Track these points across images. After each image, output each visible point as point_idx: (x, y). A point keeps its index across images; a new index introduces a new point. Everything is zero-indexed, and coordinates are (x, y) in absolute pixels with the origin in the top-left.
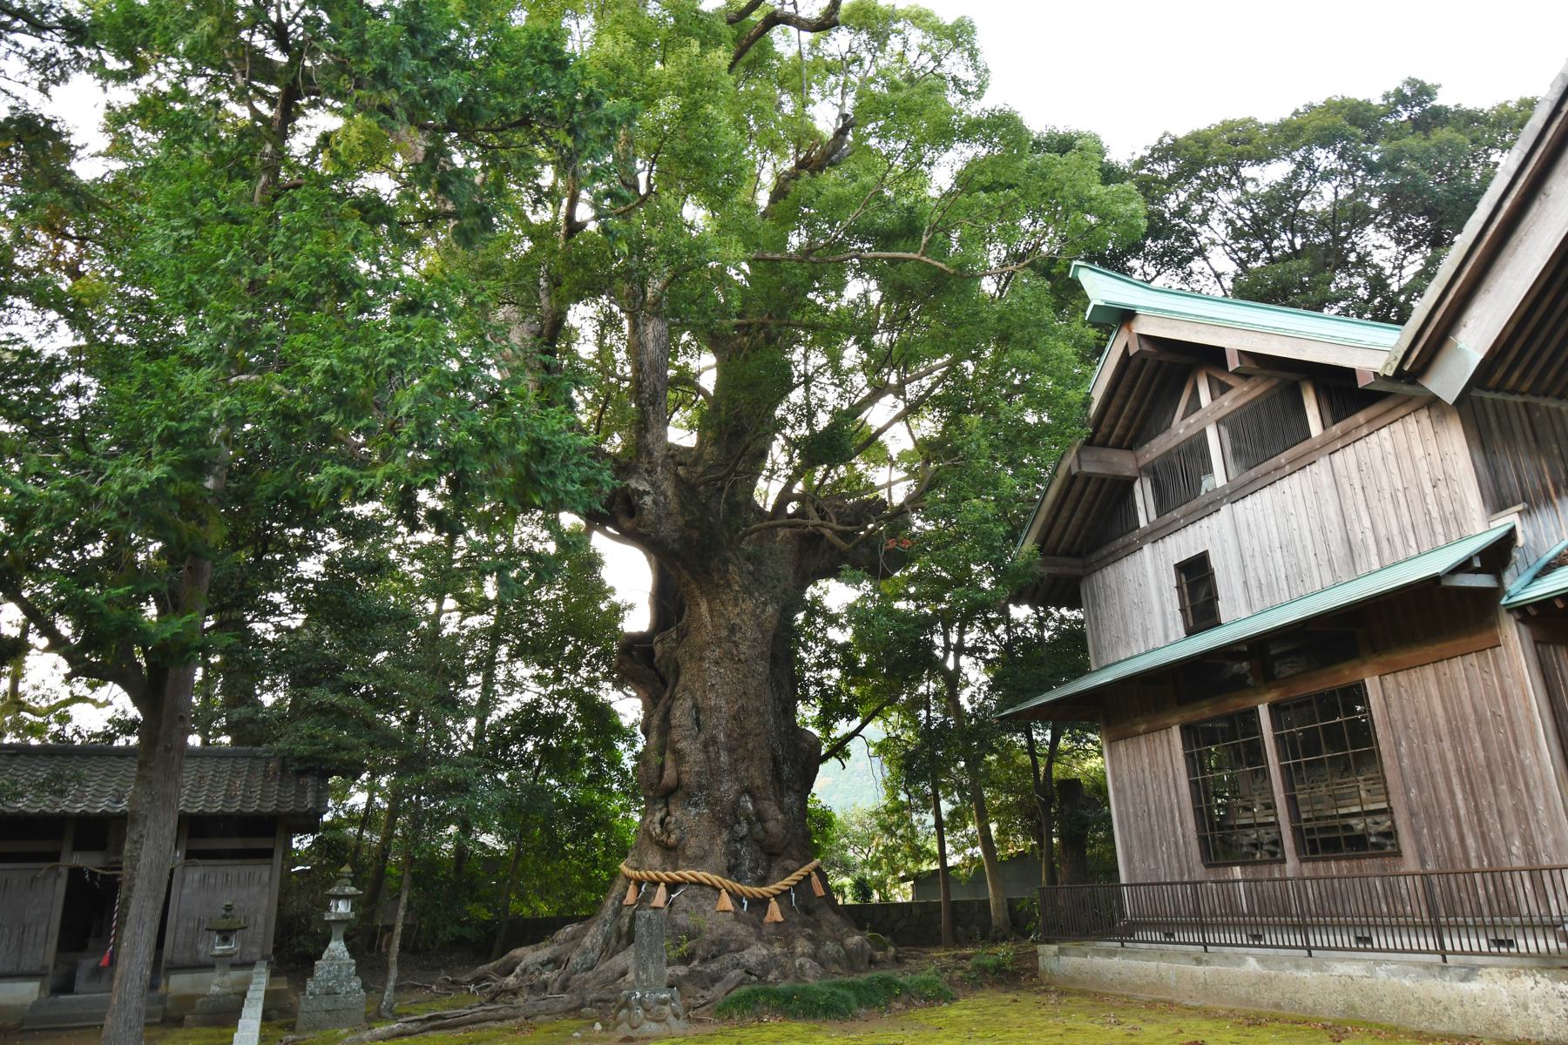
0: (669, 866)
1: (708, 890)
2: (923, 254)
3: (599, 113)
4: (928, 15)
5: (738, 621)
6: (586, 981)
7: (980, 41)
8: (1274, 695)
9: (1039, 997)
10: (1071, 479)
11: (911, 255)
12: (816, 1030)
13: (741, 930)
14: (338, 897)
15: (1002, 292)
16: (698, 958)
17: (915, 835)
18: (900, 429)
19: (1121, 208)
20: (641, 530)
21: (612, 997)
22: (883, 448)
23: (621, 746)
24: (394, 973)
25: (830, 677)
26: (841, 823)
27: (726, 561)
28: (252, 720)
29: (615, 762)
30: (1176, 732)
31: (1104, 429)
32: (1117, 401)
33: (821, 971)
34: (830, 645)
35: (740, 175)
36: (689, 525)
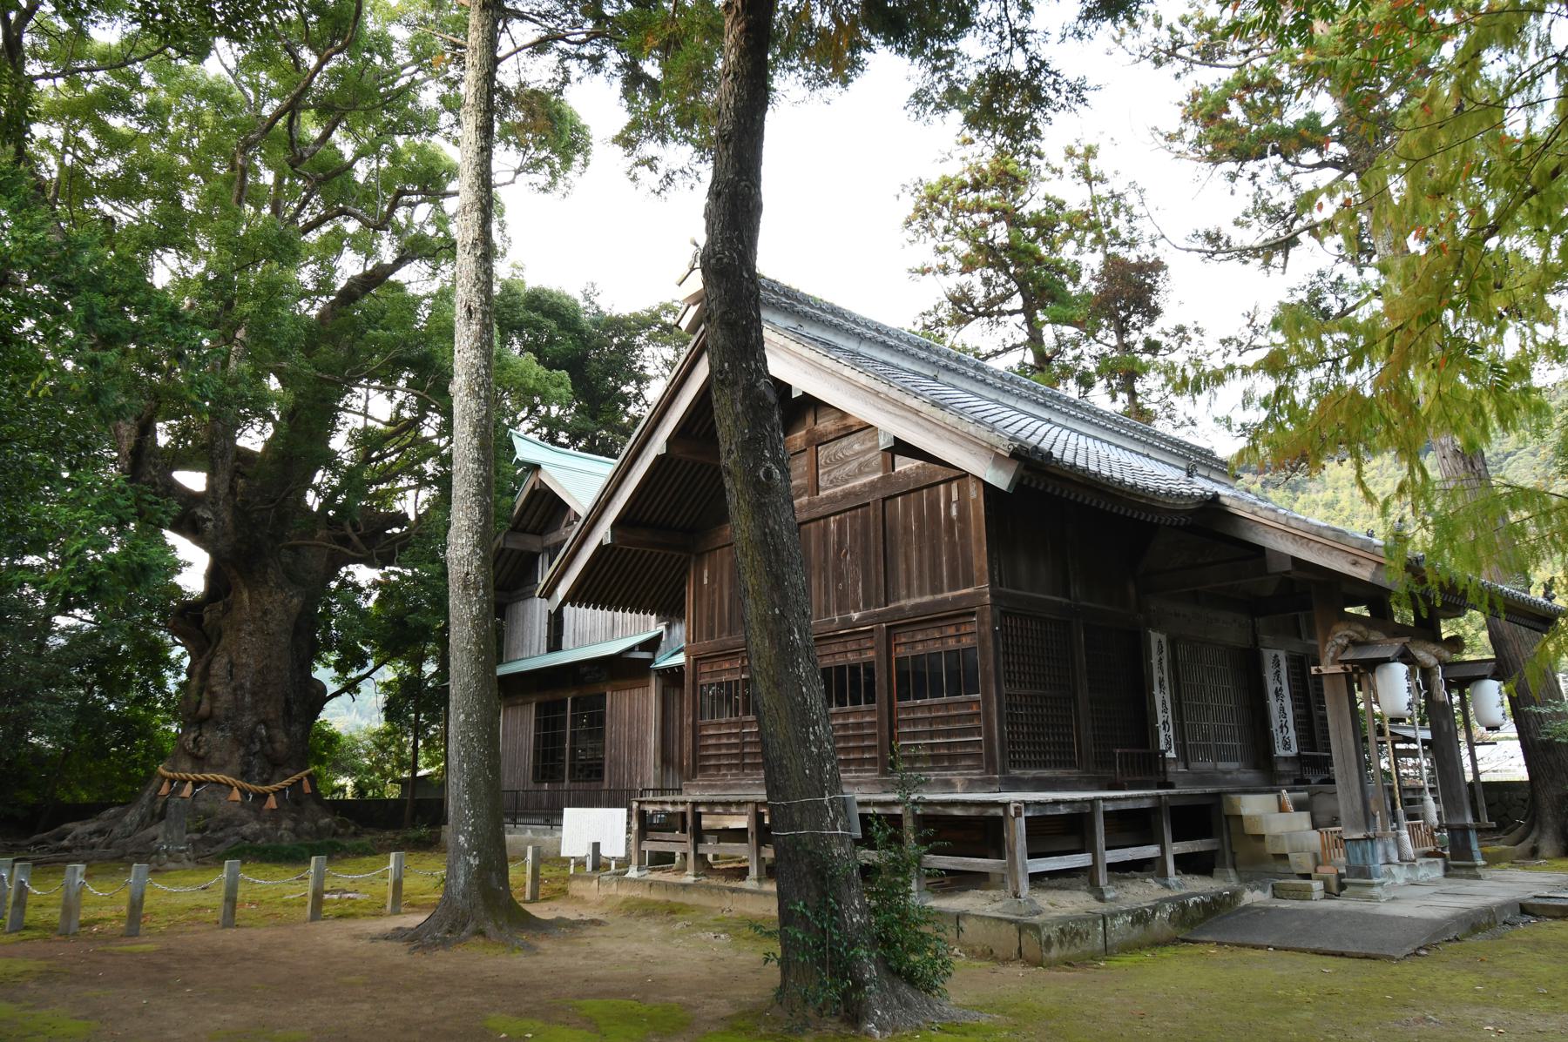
8: (574, 693)
13: (244, 813)
29: (161, 686)
31: (524, 522)
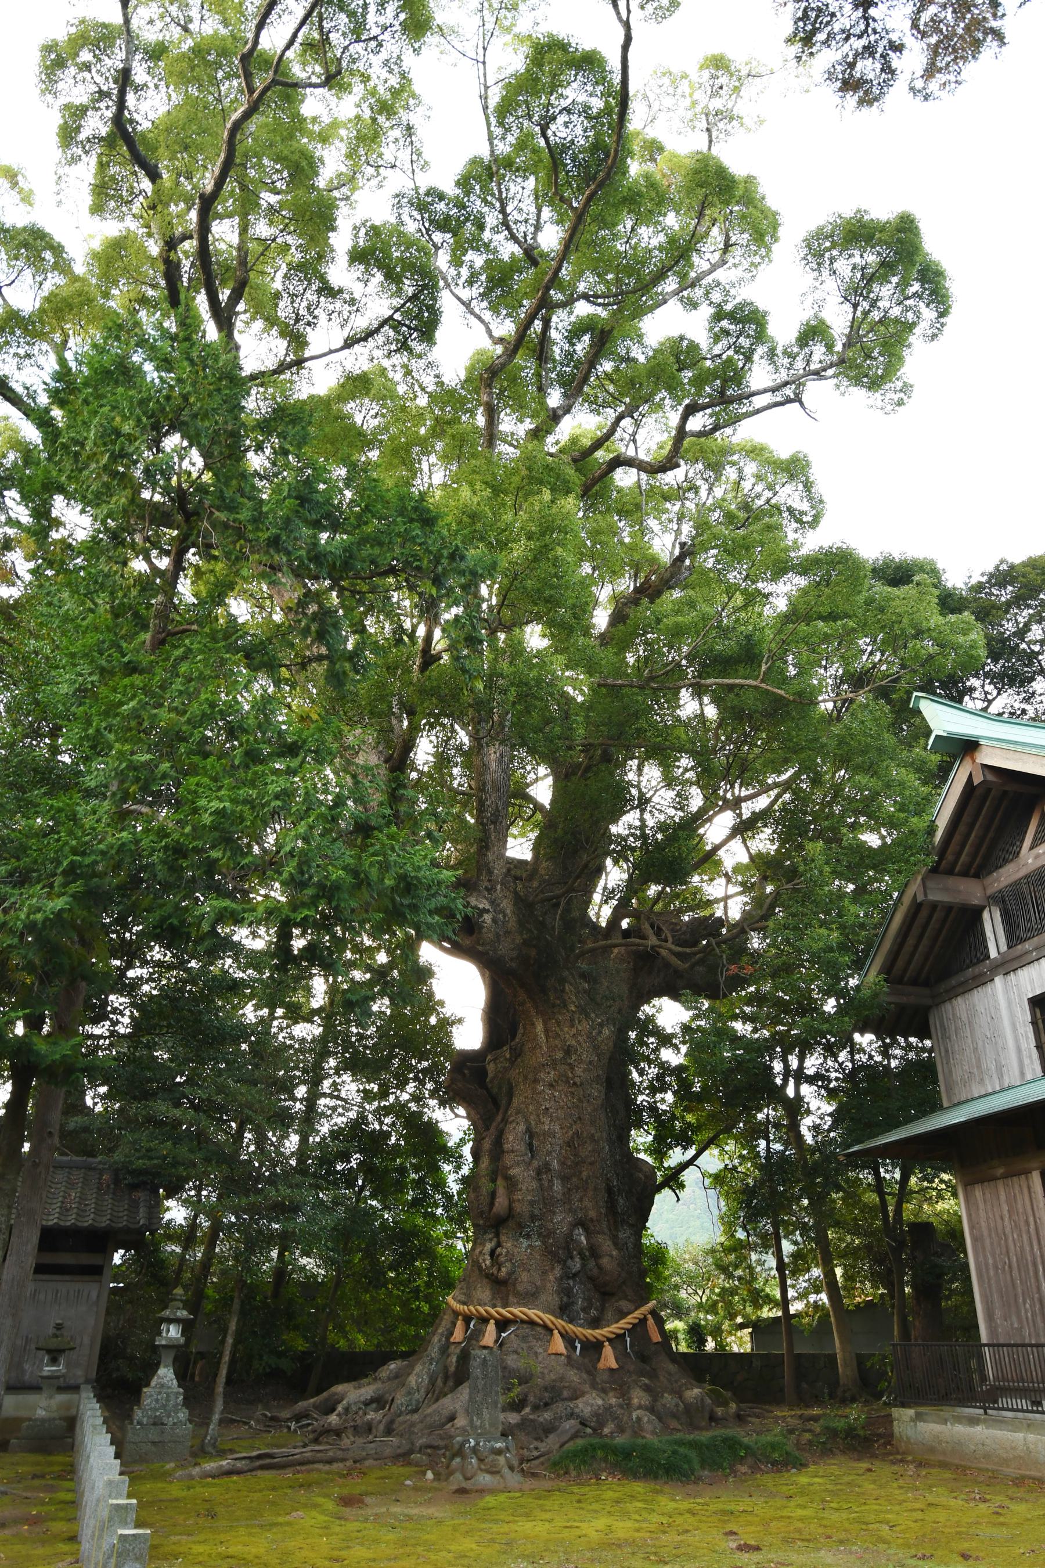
0: (499, 1302)
1: (540, 1330)
2: (762, 681)
3: (463, 566)
4: (762, 449)
5: (574, 1042)
6: (413, 1425)
7: (816, 473)
9: (895, 1468)
10: (916, 907)
11: (750, 682)
12: (657, 1492)
13: (574, 1376)
14: (170, 1321)
15: (839, 712)
16: (532, 1405)
17: (753, 1277)
18: (736, 844)
19: (961, 639)
20: (480, 948)
21: (441, 1443)
22: (719, 863)
23: (447, 1168)
24: (219, 1405)
25: (663, 1100)
26: (673, 1260)
27: (562, 981)
28: (86, 1129)
29: (440, 1185)
30: (1036, 1177)
31: (949, 857)
32: (962, 828)
33: (658, 1426)
34: (664, 1066)
35: (583, 608)
36: (525, 943)
